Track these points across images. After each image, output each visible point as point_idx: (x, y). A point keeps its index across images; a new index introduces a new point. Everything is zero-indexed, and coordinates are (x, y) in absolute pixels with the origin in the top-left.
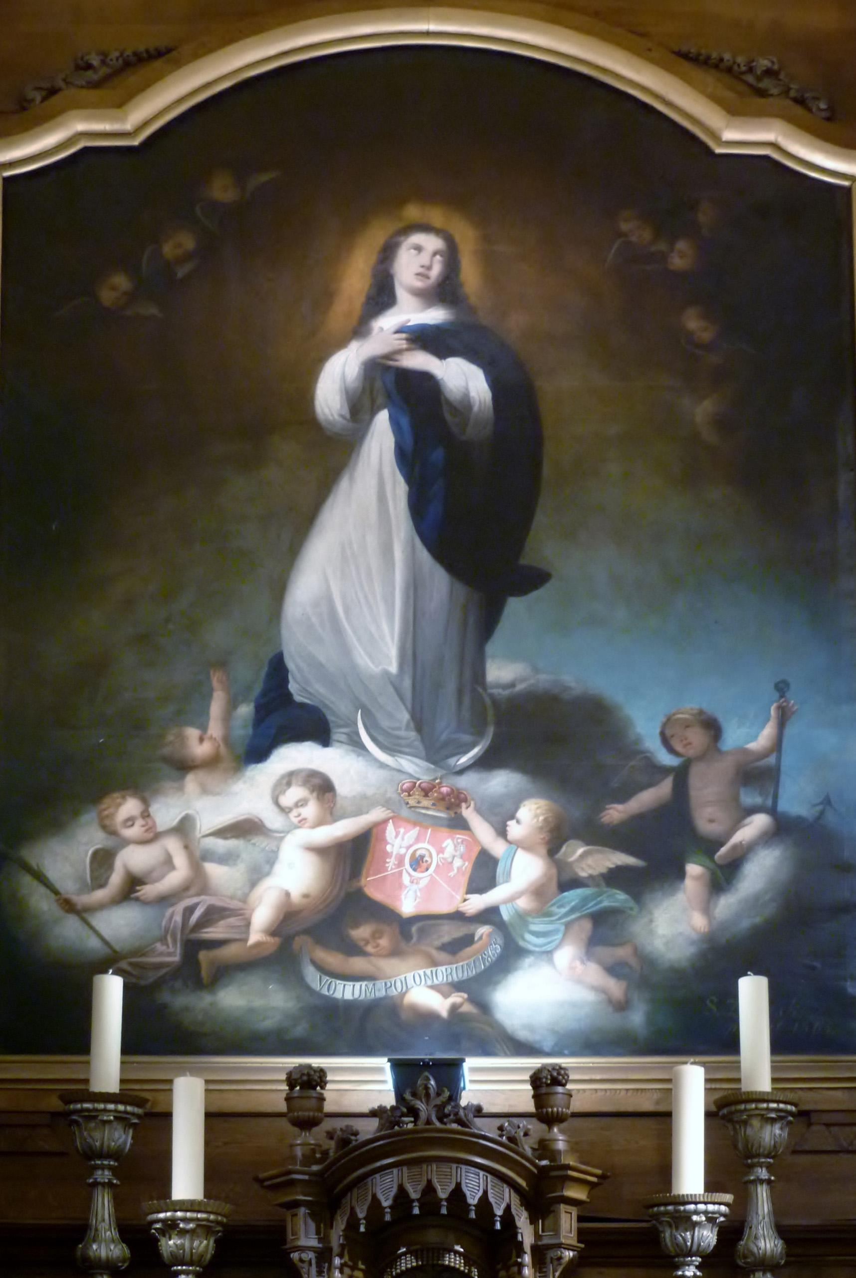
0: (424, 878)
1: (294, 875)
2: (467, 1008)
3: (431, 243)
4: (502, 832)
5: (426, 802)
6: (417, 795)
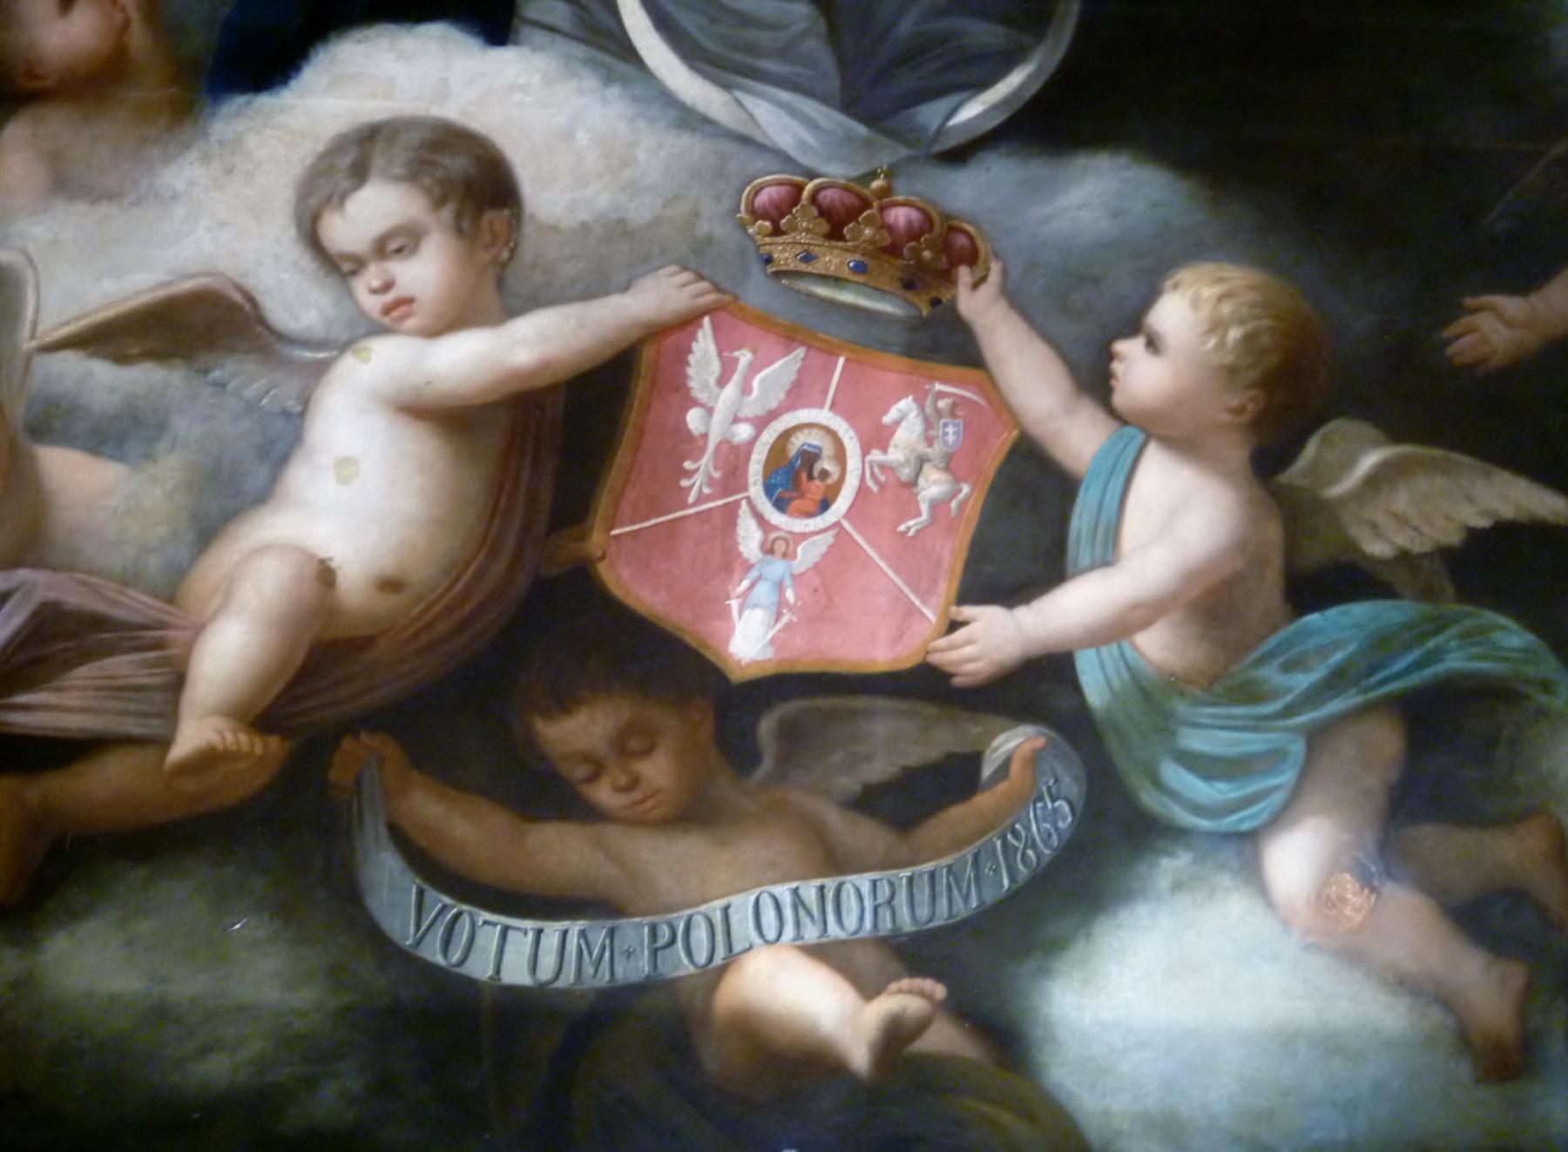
0: (811, 534)
1: (355, 499)
2: (944, 1038)
4: (1094, 380)
5: (832, 259)
6: (805, 227)
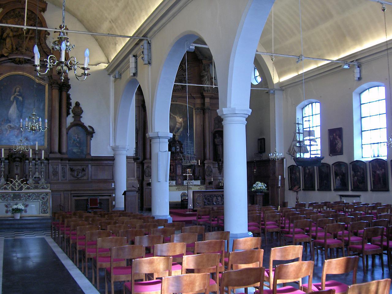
3: (19, 88)
